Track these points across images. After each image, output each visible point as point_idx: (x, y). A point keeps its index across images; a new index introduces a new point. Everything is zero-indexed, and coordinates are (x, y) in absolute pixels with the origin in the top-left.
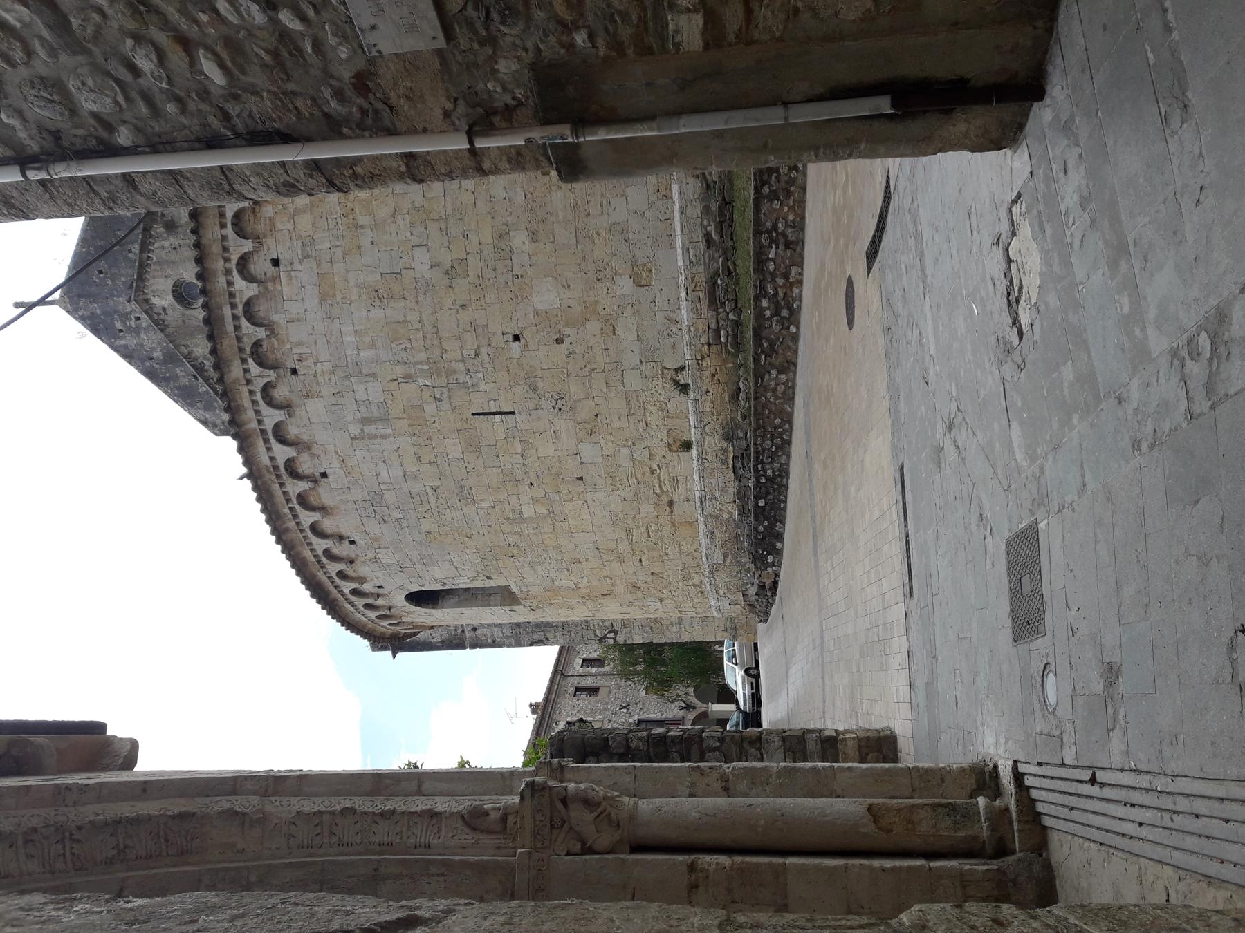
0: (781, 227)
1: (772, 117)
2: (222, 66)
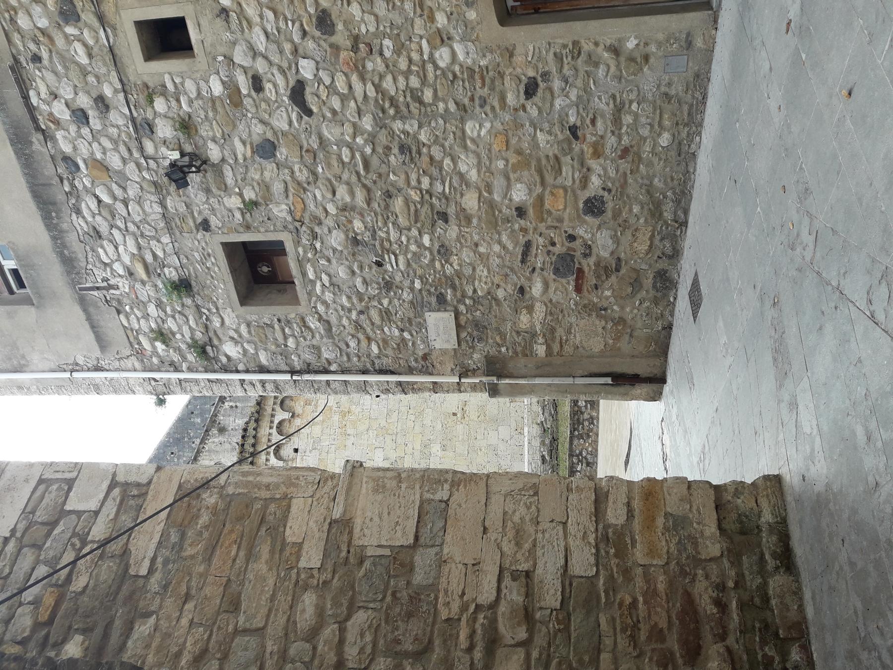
0: (584, 454)
1: (569, 381)
2: (379, 347)
